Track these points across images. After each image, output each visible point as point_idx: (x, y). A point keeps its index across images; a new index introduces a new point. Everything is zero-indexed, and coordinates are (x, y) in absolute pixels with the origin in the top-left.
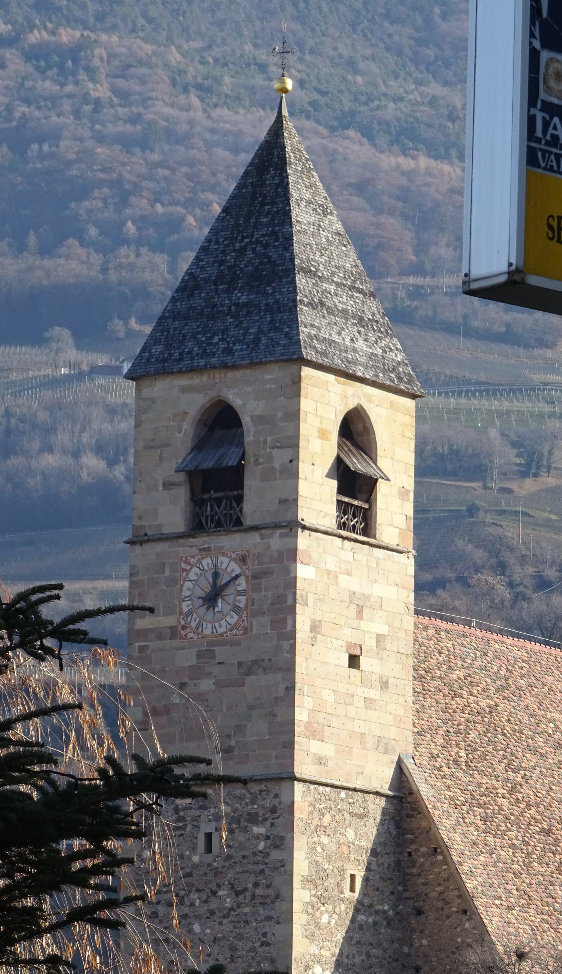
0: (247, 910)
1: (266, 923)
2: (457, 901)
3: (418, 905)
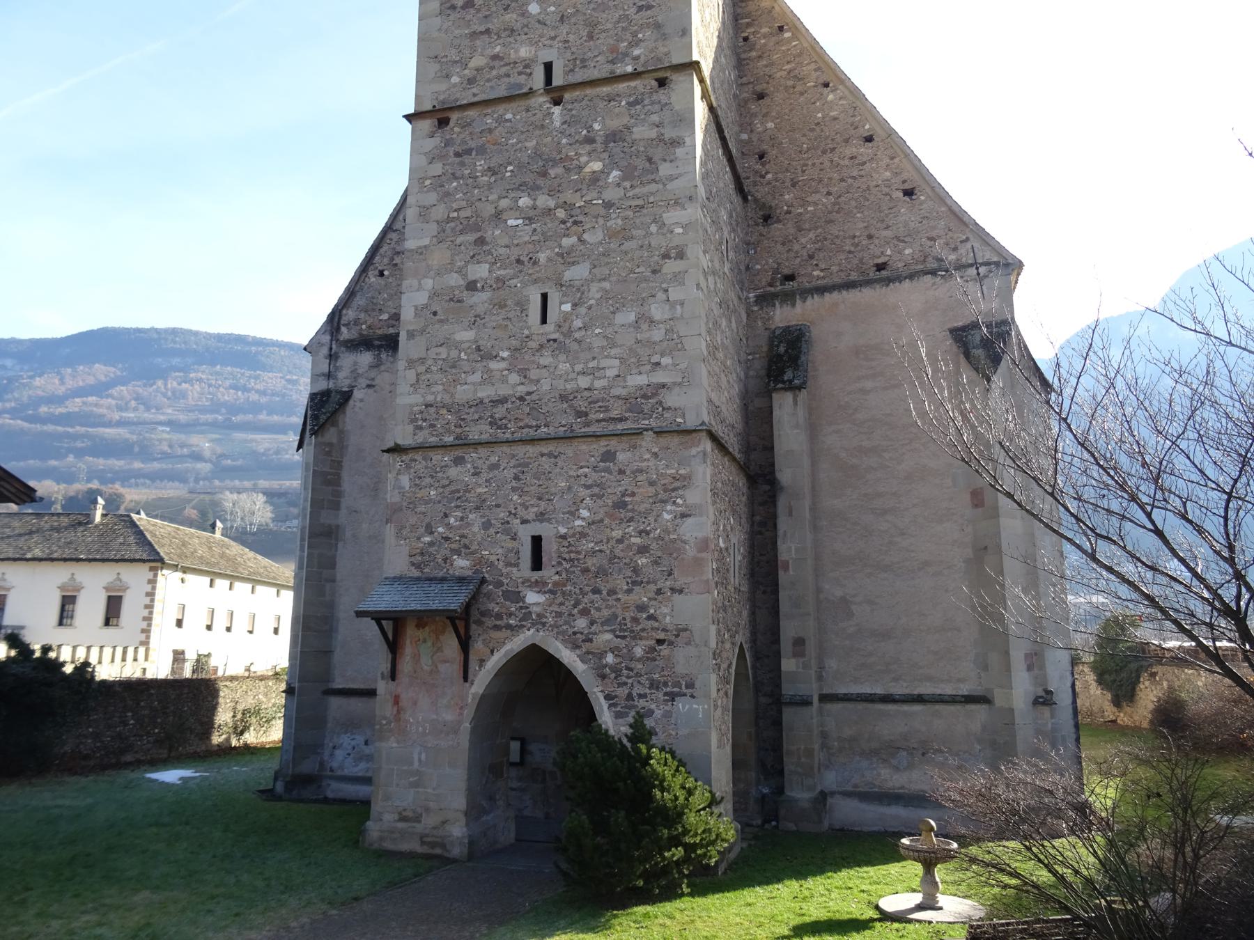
2: (814, 75)
3: (759, 88)
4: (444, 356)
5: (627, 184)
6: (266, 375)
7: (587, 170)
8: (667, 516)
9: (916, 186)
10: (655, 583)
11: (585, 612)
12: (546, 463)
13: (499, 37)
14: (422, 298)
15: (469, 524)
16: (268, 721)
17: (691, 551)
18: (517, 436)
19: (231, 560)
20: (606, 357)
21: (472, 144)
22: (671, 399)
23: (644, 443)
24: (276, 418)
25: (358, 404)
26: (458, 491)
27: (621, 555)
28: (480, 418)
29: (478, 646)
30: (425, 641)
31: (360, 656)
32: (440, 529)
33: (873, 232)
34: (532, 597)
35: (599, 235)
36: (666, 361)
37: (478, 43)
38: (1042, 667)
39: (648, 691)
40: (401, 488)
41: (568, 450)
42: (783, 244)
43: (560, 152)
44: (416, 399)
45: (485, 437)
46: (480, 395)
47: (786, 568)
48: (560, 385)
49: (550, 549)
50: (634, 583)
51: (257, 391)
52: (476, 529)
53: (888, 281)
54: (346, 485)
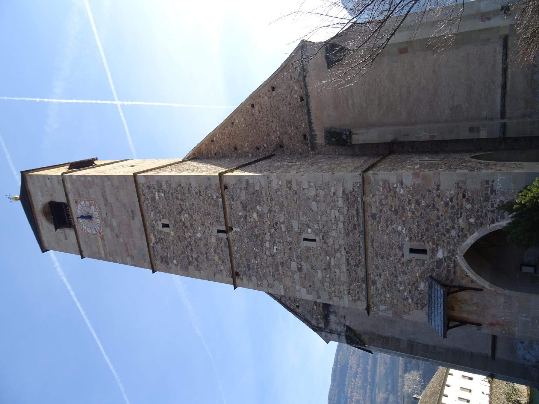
0: (187, 204)
1: (192, 192)
2: (229, 128)
3: (233, 150)
4: (328, 284)
5: (262, 203)
6: (351, 363)
7: (256, 219)
8: (402, 192)
9: (271, 86)
10: (434, 198)
11: (448, 231)
12: (376, 244)
13: (208, 249)
14: (304, 291)
15: (404, 281)
16: (515, 390)
17: (419, 181)
18: (363, 256)
19: (433, 393)
20: (330, 215)
21: (245, 264)
22: (349, 188)
23: (368, 201)
24: (370, 362)
25: (352, 324)
26: (388, 284)
27: (420, 213)
28: (355, 271)
29: (464, 282)
30: (461, 307)
31: (459, 337)
32: (406, 294)
33: (288, 103)
34: (440, 255)
35: (281, 215)
36: (333, 190)
37: (210, 257)
38: (489, 13)
39: (490, 203)
40: (385, 310)
41: (370, 234)
42: (291, 139)
43: (249, 229)
44: (346, 298)
45: (364, 270)
46: (345, 270)
47: (434, 136)
48: (342, 235)
49: (416, 245)
50: (434, 207)
51: (358, 368)
52: (406, 278)
53: (307, 95)
54: (389, 334)
